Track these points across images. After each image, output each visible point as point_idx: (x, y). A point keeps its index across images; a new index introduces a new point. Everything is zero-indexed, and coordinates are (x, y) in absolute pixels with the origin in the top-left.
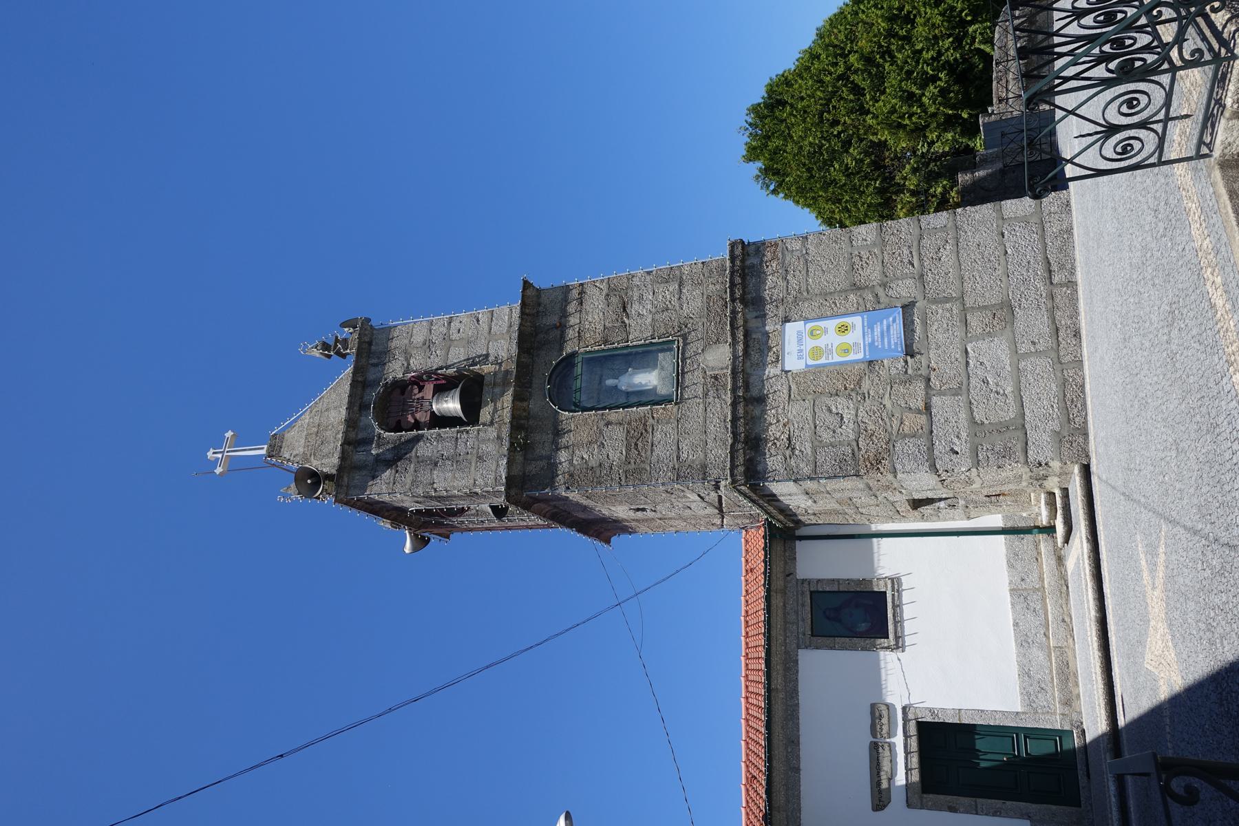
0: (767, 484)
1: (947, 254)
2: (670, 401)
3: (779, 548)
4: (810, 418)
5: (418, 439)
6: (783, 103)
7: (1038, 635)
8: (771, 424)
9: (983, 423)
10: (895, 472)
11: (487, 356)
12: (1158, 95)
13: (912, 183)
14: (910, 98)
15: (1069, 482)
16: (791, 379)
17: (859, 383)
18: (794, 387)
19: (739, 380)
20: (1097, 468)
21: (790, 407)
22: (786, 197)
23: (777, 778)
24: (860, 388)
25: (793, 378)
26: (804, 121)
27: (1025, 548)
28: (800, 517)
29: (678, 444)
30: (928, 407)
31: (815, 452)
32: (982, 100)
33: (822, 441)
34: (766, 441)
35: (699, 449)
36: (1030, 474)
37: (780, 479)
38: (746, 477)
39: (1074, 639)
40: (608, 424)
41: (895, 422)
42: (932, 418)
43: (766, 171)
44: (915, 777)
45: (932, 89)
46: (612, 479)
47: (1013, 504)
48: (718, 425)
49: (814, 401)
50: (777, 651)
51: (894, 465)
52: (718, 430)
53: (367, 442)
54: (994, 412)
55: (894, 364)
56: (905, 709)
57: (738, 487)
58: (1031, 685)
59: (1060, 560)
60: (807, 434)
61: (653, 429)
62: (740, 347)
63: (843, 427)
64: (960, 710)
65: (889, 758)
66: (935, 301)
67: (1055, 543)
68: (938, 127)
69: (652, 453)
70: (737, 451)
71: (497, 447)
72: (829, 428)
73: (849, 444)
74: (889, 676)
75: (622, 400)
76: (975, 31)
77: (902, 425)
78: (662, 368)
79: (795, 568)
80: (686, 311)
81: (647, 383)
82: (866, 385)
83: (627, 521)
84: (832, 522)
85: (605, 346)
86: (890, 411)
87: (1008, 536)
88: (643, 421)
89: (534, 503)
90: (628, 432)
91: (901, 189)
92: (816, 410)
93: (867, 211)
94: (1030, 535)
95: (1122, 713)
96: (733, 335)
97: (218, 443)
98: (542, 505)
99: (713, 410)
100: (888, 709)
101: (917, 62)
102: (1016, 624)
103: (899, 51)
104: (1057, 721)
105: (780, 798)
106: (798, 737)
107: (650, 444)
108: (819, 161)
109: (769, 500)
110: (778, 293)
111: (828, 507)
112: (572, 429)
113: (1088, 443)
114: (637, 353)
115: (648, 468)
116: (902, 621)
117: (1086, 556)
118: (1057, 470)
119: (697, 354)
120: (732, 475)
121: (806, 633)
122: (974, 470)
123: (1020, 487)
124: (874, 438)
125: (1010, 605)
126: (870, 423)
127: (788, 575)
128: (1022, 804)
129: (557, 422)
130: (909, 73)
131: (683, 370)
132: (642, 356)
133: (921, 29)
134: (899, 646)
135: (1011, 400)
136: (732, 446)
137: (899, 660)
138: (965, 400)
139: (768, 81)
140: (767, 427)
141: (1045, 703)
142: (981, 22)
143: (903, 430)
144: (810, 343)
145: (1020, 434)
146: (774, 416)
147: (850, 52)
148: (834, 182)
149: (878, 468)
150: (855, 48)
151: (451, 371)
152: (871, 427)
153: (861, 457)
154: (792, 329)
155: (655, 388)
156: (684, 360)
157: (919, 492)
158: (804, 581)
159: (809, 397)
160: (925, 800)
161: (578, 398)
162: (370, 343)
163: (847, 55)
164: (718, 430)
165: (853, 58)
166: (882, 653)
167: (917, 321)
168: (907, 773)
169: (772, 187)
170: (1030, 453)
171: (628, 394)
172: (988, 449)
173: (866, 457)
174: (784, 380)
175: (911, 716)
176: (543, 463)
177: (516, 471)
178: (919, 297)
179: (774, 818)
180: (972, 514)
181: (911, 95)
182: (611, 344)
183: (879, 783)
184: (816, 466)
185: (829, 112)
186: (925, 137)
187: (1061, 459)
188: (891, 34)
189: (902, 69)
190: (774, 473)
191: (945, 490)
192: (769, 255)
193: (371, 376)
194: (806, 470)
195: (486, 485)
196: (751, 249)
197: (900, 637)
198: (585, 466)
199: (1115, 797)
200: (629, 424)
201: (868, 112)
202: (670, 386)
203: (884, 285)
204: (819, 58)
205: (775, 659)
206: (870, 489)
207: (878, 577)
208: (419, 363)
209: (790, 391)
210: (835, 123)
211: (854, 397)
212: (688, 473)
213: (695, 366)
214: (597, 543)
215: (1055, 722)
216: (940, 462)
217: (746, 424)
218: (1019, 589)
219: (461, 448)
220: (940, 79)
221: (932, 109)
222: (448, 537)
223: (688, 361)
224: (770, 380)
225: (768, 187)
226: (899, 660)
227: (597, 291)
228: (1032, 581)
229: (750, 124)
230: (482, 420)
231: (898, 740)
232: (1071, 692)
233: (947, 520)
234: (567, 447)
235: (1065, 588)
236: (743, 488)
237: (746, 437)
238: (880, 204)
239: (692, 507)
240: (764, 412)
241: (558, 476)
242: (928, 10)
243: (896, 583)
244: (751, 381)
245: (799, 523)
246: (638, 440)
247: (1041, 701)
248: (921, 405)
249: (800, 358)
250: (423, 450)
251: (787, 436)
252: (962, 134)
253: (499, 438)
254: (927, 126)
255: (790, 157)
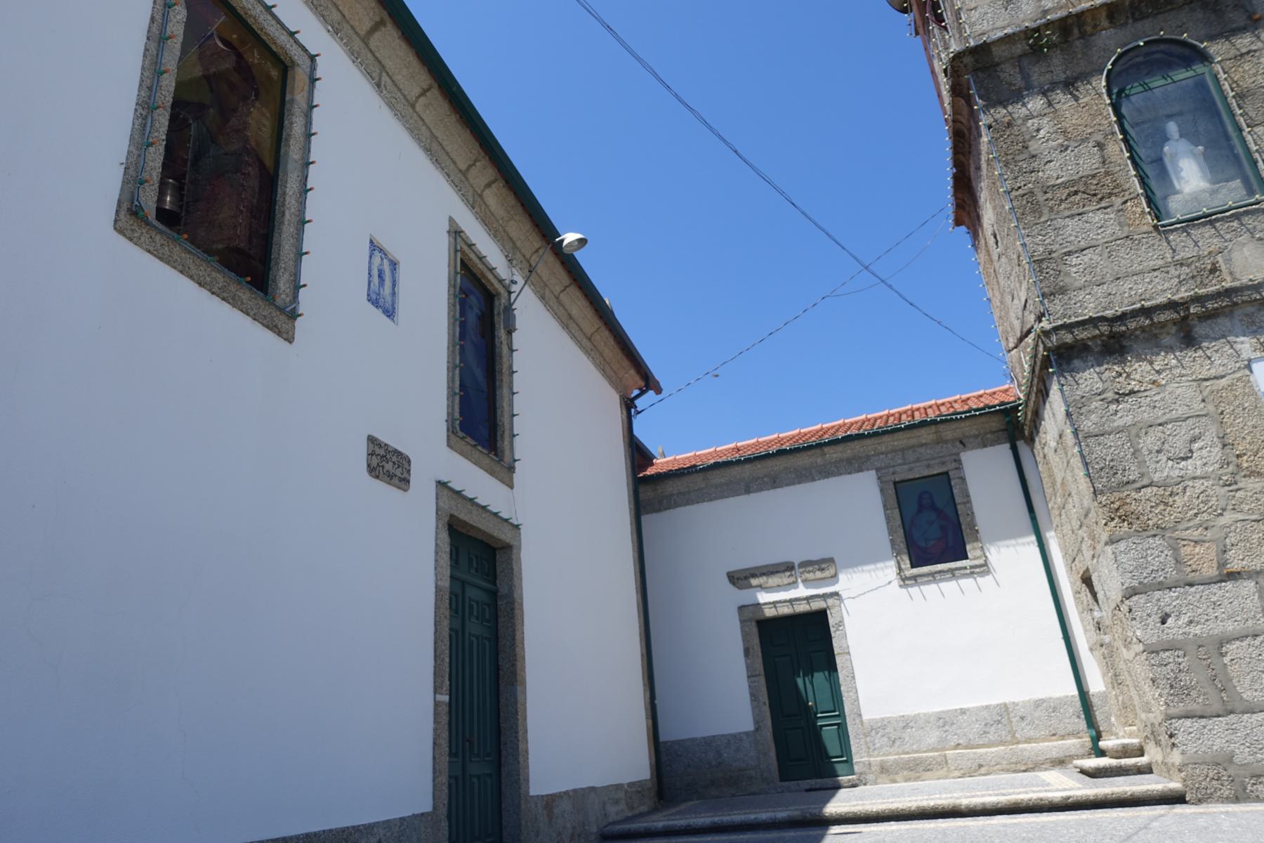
0: (1055, 378)
3: (994, 424)
4: (1174, 414)
7: (956, 737)
8: (1151, 363)
9: (1223, 655)
10: (1112, 541)
15: (1160, 775)
16: (1238, 375)
18: (1223, 382)
19: (1216, 303)
20: (1176, 814)
21: (1187, 384)
23: (735, 471)
24: (1245, 476)
25: (1239, 379)
27: (1067, 721)
28: (1037, 439)
29: (1089, 248)
30: (1233, 576)
31: (1120, 430)
33: (1140, 438)
35: (1088, 278)
36: (1157, 724)
37: (1066, 393)
38: (1059, 347)
39: (960, 777)
40: (1100, 146)
41: (1196, 533)
42: (1214, 583)
44: (769, 612)
46: (1016, 178)
47: (1120, 703)
48: (1133, 293)
49: (1205, 415)
50: (867, 446)
51: (1122, 539)
52: (1126, 295)
54: (1247, 670)
56: (836, 594)
57: (1040, 340)
58: (895, 730)
59: (1060, 762)
60: (1146, 416)
61: (1105, 208)
63: (1170, 463)
64: (849, 653)
65: (781, 584)
67: (1082, 757)
69: (1068, 217)
70: (1096, 327)
71: (1031, 16)
72: (1163, 443)
73: (1142, 475)
74: (868, 574)
75: (1142, 152)
77: (1192, 544)
79: (973, 448)
81: (1183, 178)
83: (983, 231)
84: (1044, 482)
85: (1234, 97)
86: (1212, 524)
87: (1078, 699)
88: (1116, 191)
89: (963, 97)
90: (1094, 176)
92: (1190, 421)
94: (1086, 726)
95: (842, 831)
98: (965, 110)
99: (1157, 280)
100: (832, 577)
102: (963, 712)
104: (861, 758)
105: (717, 478)
106: (782, 487)
107: (1081, 210)
109: (1041, 391)
111: (1056, 470)
112: (1081, 101)
113: (1222, 802)
114: (1232, 148)
115: (1043, 219)
116: (935, 581)
117: (1042, 795)
118: (1170, 760)
120: (1056, 329)
121: (895, 476)
122: (1140, 647)
123: (1139, 711)
124: (1162, 507)
125: (987, 704)
126: (1186, 498)
127: (961, 442)
128: (769, 722)
129: (1086, 77)
131: (1217, 220)
134: (905, 581)
136: (1103, 319)
137: (890, 583)
138: (1259, 627)
140: (1145, 359)
141: (878, 745)
143: (1184, 546)
146: (1167, 365)
149: (1113, 519)
153: (1125, 493)
157: (1099, 581)
158: (959, 461)
159: (1211, 408)
160: (749, 623)
161: (1133, 91)
164: (1126, 295)
166: (892, 563)
168: (770, 603)
170: (1188, 722)
171: (1159, 161)
172: (1180, 664)
173: (1128, 501)
174: (1232, 365)
175: (830, 601)
176: (1019, 82)
177: (999, 53)
179: (696, 475)
180: (1096, 653)
182: (1238, 105)
183: (754, 576)
184: (1096, 436)
187: (1187, 764)
190: (1073, 383)
191: (1110, 614)
194: (1088, 424)
195: (972, 25)
197: (916, 580)
198: (1027, 137)
199: (756, 819)
200: (1107, 173)
202: (1185, 211)
205: (856, 446)
206: (1086, 515)
207: (985, 548)
209: (1216, 378)
211: (1227, 470)
212: (1047, 273)
213: (1228, 237)
214: (950, 209)
215: (860, 757)
216: (1142, 601)
217: (1143, 329)
218: (1008, 714)
222: (917, 33)
223: (1235, 224)
224: (1228, 347)
226: (890, 583)
228: (1024, 730)
231: (802, 591)
232: (897, 773)
233: (1082, 624)
234: (1050, 104)
235: (1023, 768)
236: (1041, 348)
237: (1122, 335)
239: (1015, 300)
240: (1170, 349)
241: (1005, 107)
243: (982, 569)
244: (1221, 320)
245: (1031, 441)
246: (1084, 193)
247: (880, 741)
248: (1235, 566)
251: (1136, 389)
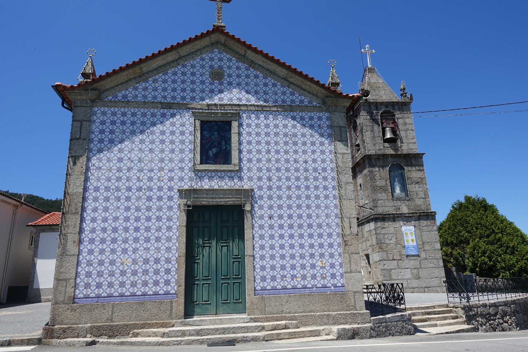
1: (432, 265)
2: (392, 197)
5: (379, 125)
6: (486, 211)
11: (403, 143)
12: (456, 296)
13: (455, 252)
14: (484, 253)
17: (399, 244)
22: (451, 211)
26: (478, 218)
30: (394, 260)
31: (382, 234)
32: (481, 274)
34: (384, 222)
40: (386, 181)
43: (461, 204)
45: (486, 260)
53: (377, 109)
55: (404, 252)
60: (386, 232)
62: (407, 215)
66: (420, 262)
68: (473, 261)
75: (392, 183)
76: (507, 273)
78: (401, 194)
80: (417, 200)
82: (399, 246)
91: (453, 249)
93: (445, 238)
96: (411, 213)
97: (371, 48)
101: (497, 255)
103: (501, 250)
108: (464, 223)
110: (422, 224)
114: (405, 187)
119: (405, 203)
130: (493, 253)
132: (404, 189)
133: (509, 257)
135: (397, 278)
139: (495, 205)
142: (510, 276)
144: (409, 232)
145: (389, 279)
147: (503, 234)
148: (456, 228)
150: (504, 236)
151: (398, 132)
152: (389, 247)
154: (412, 228)
155: (395, 192)
156: (403, 200)
162: (405, 105)
163: (501, 233)
165: (500, 235)
167: (415, 258)
169: (455, 206)
171: (394, 184)
174: (399, 226)
178: (421, 258)
181: (485, 253)
185: (481, 227)
186: (471, 257)
188: (508, 247)
189: (495, 250)
192: (432, 222)
193: (396, 107)
196: (433, 217)
201: (480, 239)
203: (424, 250)
204: (501, 223)
208: (400, 122)
210: (477, 229)
219: (377, 138)
220: (490, 262)
221: (479, 260)
225: (455, 204)
227: (422, 175)
229: (479, 199)
230: (385, 143)
238: (447, 242)
240: (391, 221)
242: (515, 259)
248: (395, 258)
249: (405, 230)
250: (376, 127)
252: (471, 268)
253: (380, 150)
254: (474, 258)
255: (465, 213)
